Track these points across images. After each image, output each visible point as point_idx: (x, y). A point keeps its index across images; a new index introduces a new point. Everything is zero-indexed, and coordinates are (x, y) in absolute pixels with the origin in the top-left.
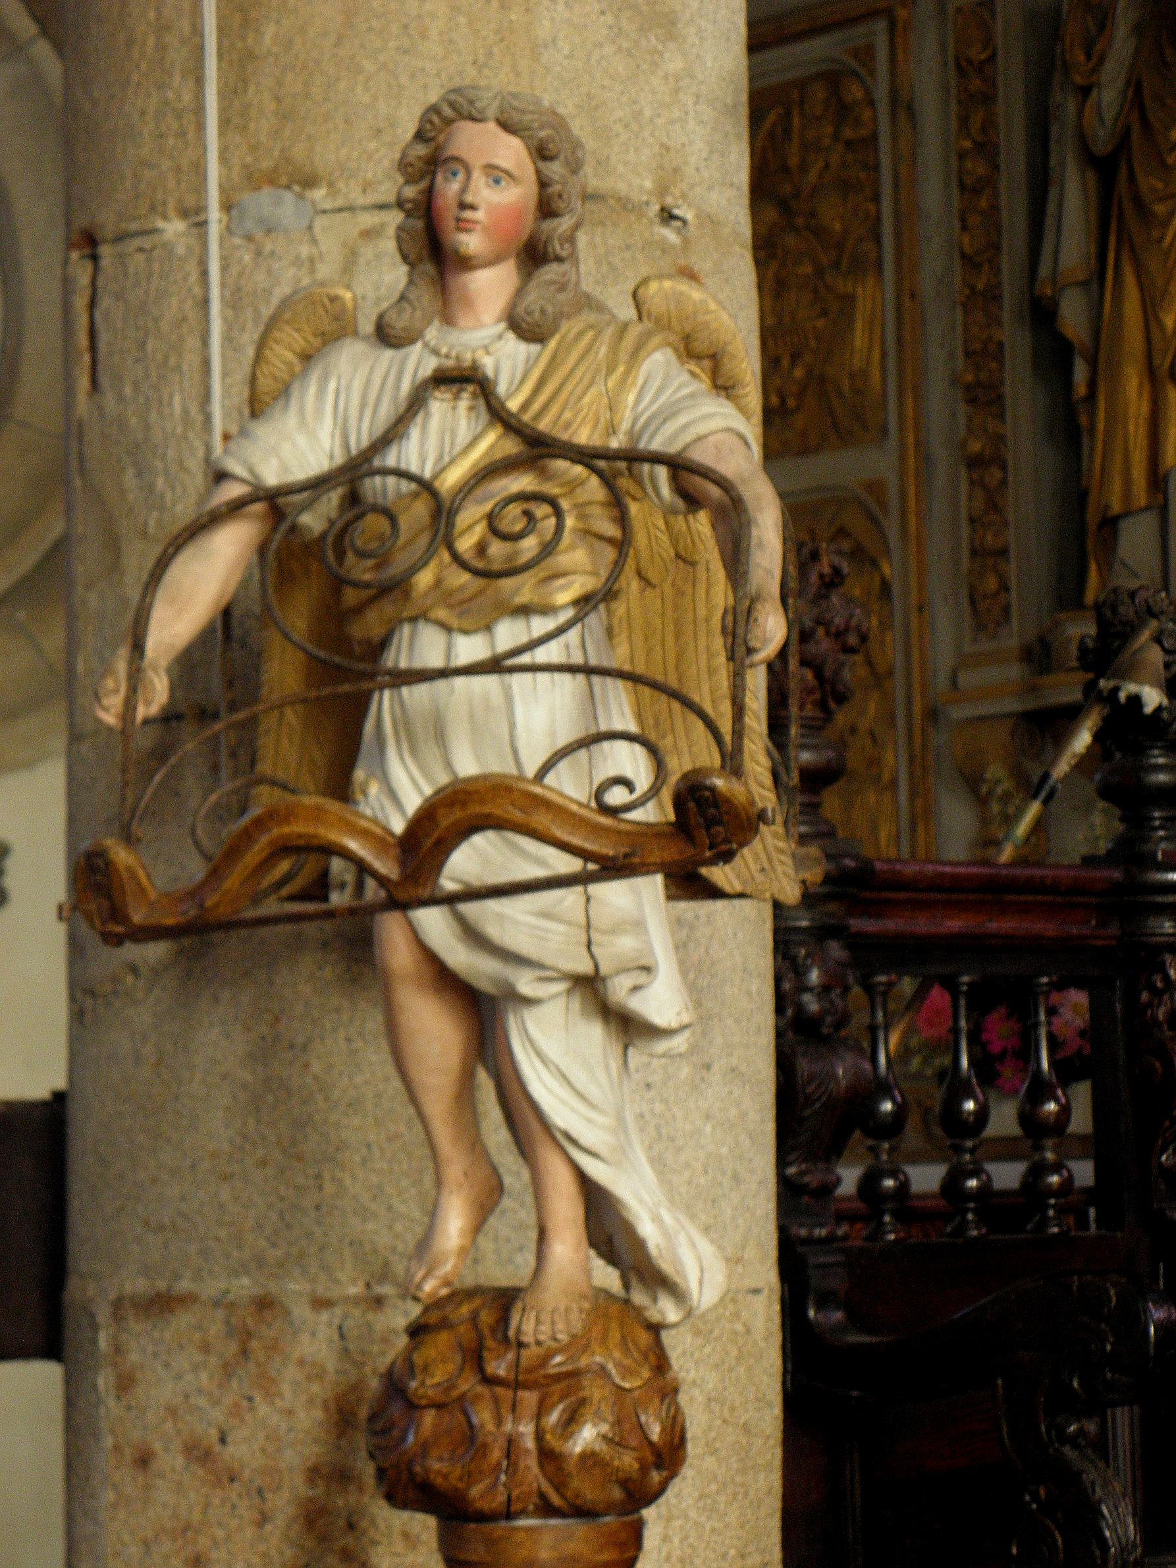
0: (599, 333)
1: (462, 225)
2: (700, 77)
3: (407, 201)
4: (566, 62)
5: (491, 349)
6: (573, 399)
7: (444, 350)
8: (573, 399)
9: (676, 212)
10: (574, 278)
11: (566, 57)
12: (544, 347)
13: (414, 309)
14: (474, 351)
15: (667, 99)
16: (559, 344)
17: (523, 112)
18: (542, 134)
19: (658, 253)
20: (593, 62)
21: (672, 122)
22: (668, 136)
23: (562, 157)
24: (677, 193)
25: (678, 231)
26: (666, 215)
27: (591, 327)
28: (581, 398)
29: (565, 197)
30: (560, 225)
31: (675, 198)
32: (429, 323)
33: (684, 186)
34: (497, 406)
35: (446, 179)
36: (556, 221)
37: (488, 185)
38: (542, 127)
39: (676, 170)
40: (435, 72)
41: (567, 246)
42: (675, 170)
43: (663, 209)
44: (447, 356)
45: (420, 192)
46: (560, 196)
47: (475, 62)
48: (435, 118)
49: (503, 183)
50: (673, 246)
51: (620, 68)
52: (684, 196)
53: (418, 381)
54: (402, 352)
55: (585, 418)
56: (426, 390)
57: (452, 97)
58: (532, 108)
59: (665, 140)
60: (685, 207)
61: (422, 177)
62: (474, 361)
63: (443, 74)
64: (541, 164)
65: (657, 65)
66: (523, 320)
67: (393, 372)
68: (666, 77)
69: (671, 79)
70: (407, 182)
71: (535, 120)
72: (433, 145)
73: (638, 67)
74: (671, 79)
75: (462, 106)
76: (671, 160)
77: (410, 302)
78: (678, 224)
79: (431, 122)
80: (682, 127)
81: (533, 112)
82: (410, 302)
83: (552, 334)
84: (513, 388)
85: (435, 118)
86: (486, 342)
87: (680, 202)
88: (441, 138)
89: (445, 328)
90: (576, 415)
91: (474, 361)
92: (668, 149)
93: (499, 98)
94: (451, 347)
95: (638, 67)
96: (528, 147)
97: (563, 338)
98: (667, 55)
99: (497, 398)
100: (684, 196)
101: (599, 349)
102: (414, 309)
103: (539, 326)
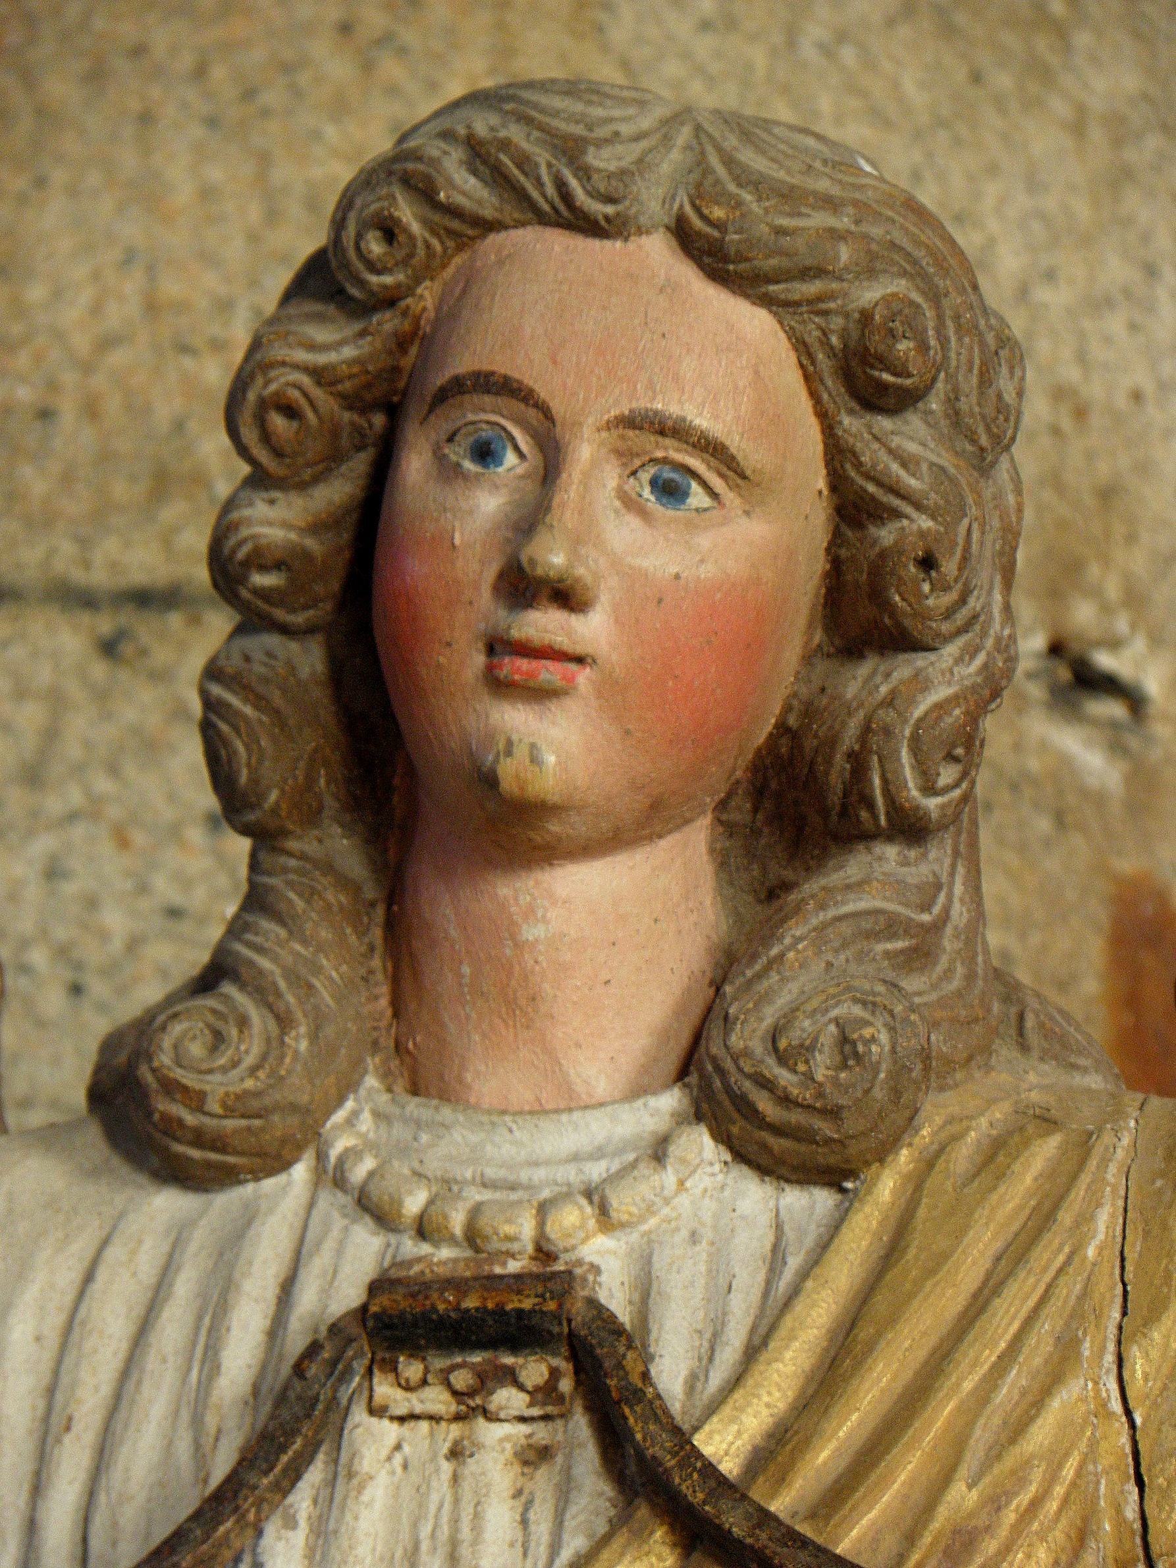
0: (1083, 1146)
1: (515, 667)
2: (132, 286)
3: (260, 560)
4: (703, 46)
5: (622, 1202)
6: (981, 1437)
7: (414, 1203)
8: (981, 1437)
9: (1105, 661)
10: (960, 914)
11: (705, 26)
12: (848, 1202)
13: (284, 1022)
14: (543, 1210)
15: (1082, 209)
16: (917, 1184)
17: (790, 197)
18: (869, 294)
19: (1043, 824)
20: (808, 51)
21: (1101, 304)
22: (1082, 358)
23: (934, 404)
24: (1113, 590)
25: (1116, 747)
26: (1064, 674)
27: (1047, 1122)
28: (1017, 1429)
29: (949, 566)
30: (921, 683)
31: (1106, 609)
32: (347, 1086)
33: (1138, 562)
34: (659, 1448)
35: (448, 472)
36: (904, 667)
37: (630, 503)
38: (869, 270)
39: (1108, 494)
40: (187, 61)
41: (947, 775)
42: (1108, 494)
43: (1056, 649)
44: (423, 1230)
45: (315, 528)
46: (928, 563)
47: (345, 28)
48: (407, 213)
49: (697, 497)
50: (1098, 799)
51: (909, 86)
52: (1134, 599)
53: (295, 1342)
54: (227, 1201)
55: (1036, 1504)
56: (338, 1370)
57: (483, 124)
58: (823, 185)
59: (1072, 374)
60: (1139, 644)
61: (333, 459)
62: (544, 1253)
63: (219, 73)
64: (851, 423)
65: (1045, 75)
66: (765, 1083)
67: (184, 1286)
68: (1078, 128)
69: (1096, 134)
70: (259, 480)
71: (836, 235)
72: (388, 322)
73: (976, 78)
74: (1096, 134)
75: (524, 162)
76: (1090, 456)
77: (264, 994)
78: (1112, 709)
79: (390, 231)
80: (1133, 327)
81: (830, 203)
82: (264, 994)
83: (882, 1153)
84: (717, 1378)
85: (407, 213)
86: (596, 1171)
87: (1122, 624)
88: (427, 296)
89: (414, 1106)
90: (996, 1502)
91: (544, 1253)
92: (1081, 413)
93: (684, 134)
94: (448, 1187)
95: (976, 78)
96: (801, 346)
97: (929, 1164)
98: (1083, 39)
99: (656, 1410)
100: (1134, 599)
101: (1085, 1219)
102: (284, 1022)
103: (833, 1113)
